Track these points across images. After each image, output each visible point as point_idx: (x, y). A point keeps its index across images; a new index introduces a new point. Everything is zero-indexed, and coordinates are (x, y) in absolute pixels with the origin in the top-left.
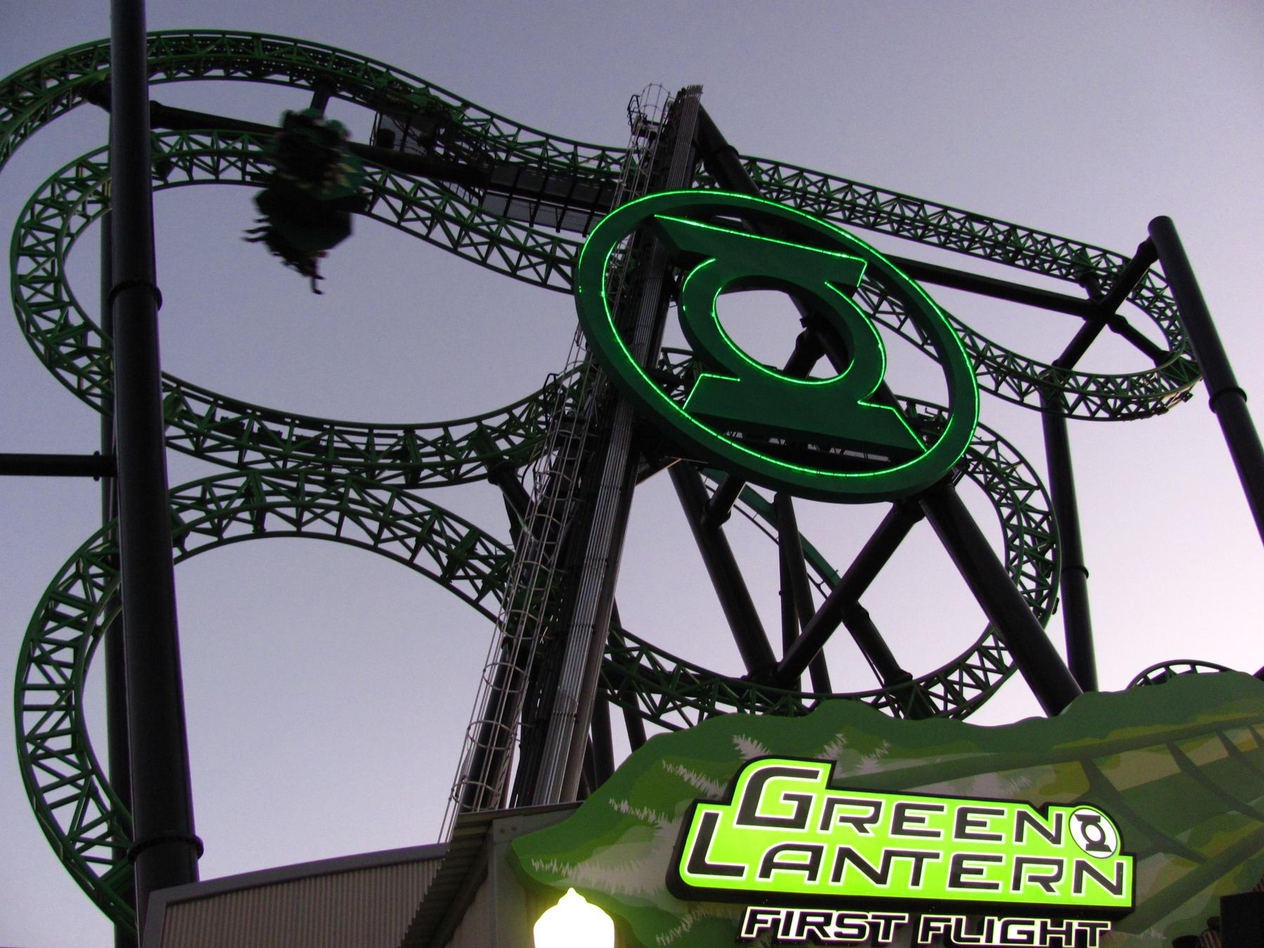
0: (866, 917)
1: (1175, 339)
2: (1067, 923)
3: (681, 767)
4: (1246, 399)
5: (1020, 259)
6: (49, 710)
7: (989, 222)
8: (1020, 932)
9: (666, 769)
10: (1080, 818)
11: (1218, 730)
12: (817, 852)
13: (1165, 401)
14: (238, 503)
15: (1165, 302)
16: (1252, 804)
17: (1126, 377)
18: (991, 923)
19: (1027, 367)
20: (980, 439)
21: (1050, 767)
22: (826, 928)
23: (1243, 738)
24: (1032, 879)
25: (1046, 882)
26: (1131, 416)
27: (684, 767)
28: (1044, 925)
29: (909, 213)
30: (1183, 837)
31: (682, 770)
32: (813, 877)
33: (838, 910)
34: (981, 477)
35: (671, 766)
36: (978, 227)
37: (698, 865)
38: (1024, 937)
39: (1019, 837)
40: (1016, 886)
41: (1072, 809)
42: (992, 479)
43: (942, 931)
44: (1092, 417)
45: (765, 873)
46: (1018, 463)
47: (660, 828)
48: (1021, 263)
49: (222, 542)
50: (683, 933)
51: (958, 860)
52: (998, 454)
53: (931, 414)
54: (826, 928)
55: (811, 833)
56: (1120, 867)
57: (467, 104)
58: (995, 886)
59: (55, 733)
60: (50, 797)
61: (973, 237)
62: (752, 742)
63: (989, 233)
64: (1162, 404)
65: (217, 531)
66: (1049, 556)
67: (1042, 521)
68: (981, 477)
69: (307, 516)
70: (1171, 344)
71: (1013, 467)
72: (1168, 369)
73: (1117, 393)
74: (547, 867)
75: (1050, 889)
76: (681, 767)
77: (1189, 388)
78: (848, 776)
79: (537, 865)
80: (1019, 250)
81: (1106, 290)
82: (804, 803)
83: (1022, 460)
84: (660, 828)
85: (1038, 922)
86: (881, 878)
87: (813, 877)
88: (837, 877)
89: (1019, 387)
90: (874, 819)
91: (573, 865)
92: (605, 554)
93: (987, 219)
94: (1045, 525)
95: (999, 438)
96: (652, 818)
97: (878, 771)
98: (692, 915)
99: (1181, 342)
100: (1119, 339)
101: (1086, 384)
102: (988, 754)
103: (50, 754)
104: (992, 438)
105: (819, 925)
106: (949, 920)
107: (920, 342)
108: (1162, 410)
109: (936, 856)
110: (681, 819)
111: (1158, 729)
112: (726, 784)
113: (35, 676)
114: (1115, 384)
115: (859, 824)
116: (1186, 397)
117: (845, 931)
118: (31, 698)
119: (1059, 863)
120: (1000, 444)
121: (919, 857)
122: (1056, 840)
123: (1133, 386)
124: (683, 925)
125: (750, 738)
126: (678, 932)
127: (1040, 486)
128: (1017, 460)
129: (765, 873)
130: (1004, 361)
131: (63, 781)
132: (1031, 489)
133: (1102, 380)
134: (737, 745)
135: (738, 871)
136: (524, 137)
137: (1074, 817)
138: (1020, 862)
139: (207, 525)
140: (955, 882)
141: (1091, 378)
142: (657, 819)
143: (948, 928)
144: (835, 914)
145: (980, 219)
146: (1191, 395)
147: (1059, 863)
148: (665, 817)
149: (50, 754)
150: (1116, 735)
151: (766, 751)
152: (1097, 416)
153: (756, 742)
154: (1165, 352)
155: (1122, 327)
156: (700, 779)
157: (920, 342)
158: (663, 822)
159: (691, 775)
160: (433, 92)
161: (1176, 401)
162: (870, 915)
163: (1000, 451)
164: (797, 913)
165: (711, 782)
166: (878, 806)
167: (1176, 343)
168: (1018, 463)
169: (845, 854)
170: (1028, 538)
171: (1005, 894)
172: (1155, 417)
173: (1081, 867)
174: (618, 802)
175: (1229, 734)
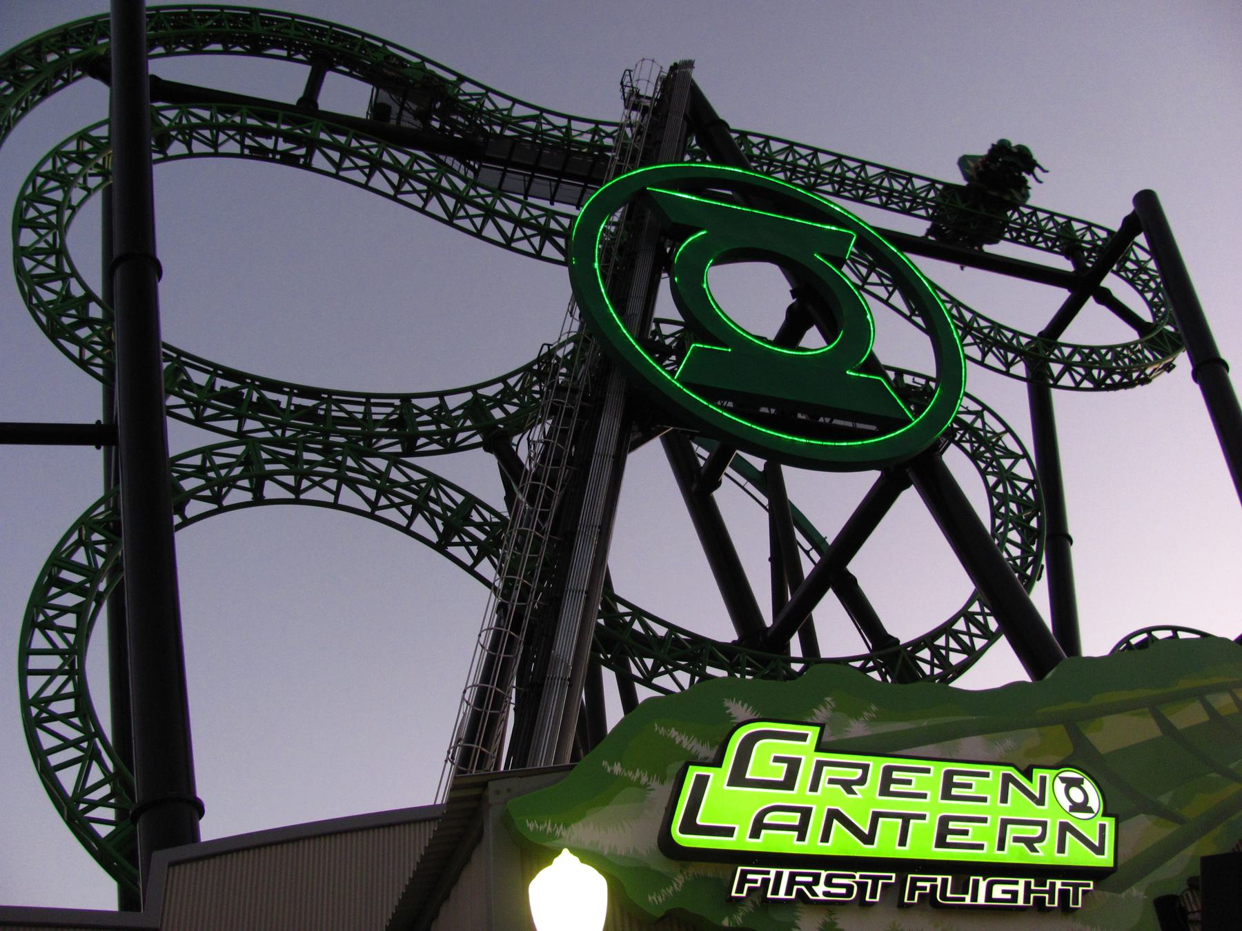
0: (854, 877)
1: (1159, 311)
2: (1050, 883)
3: (673, 729)
6: (52, 674)
8: (1004, 892)
10: (1063, 780)
12: (806, 813)
13: (1148, 371)
14: (237, 471)
17: (1110, 348)
18: (976, 883)
19: (1013, 338)
20: (967, 408)
21: (1034, 730)
24: (1016, 839)
25: (1030, 843)
26: (1115, 387)
27: (676, 730)
28: (1027, 885)
29: (897, 187)
31: (673, 733)
32: (802, 837)
33: (826, 871)
34: (967, 446)
35: (662, 728)
37: (690, 826)
38: (1009, 896)
39: (1004, 799)
40: (1001, 847)
42: (978, 448)
43: (928, 891)
44: (1077, 387)
45: (755, 834)
46: (1004, 433)
47: (652, 790)
49: (222, 509)
51: (944, 821)
52: (984, 423)
53: (919, 384)
55: (800, 795)
57: (462, 79)
59: (58, 696)
60: (54, 760)
62: (742, 705)
64: (1145, 374)
65: (217, 498)
66: (1034, 523)
67: (1027, 489)
68: (967, 446)
69: (305, 483)
70: (1154, 315)
71: (999, 436)
73: (1102, 364)
74: (541, 828)
75: (1034, 850)
76: (673, 729)
78: (836, 739)
79: (531, 826)
81: (1090, 262)
82: (794, 765)
83: (1008, 430)
84: (652, 790)
85: (1022, 881)
86: (868, 839)
87: (802, 837)
89: (1006, 357)
91: (566, 826)
92: (598, 521)
94: (1030, 493)
95: (985, 408)
96: (644, 779)
97: (868, 733)
98: (684, 876)
100: (1104, 311)
101: (1071, 355)
102: (974, 718)
103: (54, 717)
104: (979, 408)
105: (809, 886)
106: (935, 880)
108: (1146, 381)
113: (39, 641)
114: (1099, 355)
115: (847, 785)
116: (1169, 368)
118: (35, 662)
119: (1043, 824)
120: (986, 413)
121: (906, 819)
122: (1040, 801)
124: (675, 885)
125: (740, 702)
127: (1025, 455)
129: (755, 834)
130: (990, 332)
131: (67, 744)
132: (1017, 458)
133: (1086, 351)
134: (728, 708)
136: (519, 111)
138: (1005, 823)
139: (207, 493)
140: (941, 843)
141: (1076, 349)
143: (934, 888)
144: (824, 874)
146: (1174, 366)
147: (1043, 824)
148: (657, 779)
149: (54, 717)
151: (756, 715)
153: (746, 705)
154: (1149, 324)
155: (1107, 299)
156: (693, 739)
157: (908, 313)
158: (655, 784)
160: (429, 66)
161: (1159, 372)
162: (857, 875)
164: (786, 873)
166: (865, 768)
167: (1160, 315)
168: (1004, 433)
169: (833, 815)
170: (1013, 506)
171: (988, 854)
173: (1065, 828)
174: (611, 764)
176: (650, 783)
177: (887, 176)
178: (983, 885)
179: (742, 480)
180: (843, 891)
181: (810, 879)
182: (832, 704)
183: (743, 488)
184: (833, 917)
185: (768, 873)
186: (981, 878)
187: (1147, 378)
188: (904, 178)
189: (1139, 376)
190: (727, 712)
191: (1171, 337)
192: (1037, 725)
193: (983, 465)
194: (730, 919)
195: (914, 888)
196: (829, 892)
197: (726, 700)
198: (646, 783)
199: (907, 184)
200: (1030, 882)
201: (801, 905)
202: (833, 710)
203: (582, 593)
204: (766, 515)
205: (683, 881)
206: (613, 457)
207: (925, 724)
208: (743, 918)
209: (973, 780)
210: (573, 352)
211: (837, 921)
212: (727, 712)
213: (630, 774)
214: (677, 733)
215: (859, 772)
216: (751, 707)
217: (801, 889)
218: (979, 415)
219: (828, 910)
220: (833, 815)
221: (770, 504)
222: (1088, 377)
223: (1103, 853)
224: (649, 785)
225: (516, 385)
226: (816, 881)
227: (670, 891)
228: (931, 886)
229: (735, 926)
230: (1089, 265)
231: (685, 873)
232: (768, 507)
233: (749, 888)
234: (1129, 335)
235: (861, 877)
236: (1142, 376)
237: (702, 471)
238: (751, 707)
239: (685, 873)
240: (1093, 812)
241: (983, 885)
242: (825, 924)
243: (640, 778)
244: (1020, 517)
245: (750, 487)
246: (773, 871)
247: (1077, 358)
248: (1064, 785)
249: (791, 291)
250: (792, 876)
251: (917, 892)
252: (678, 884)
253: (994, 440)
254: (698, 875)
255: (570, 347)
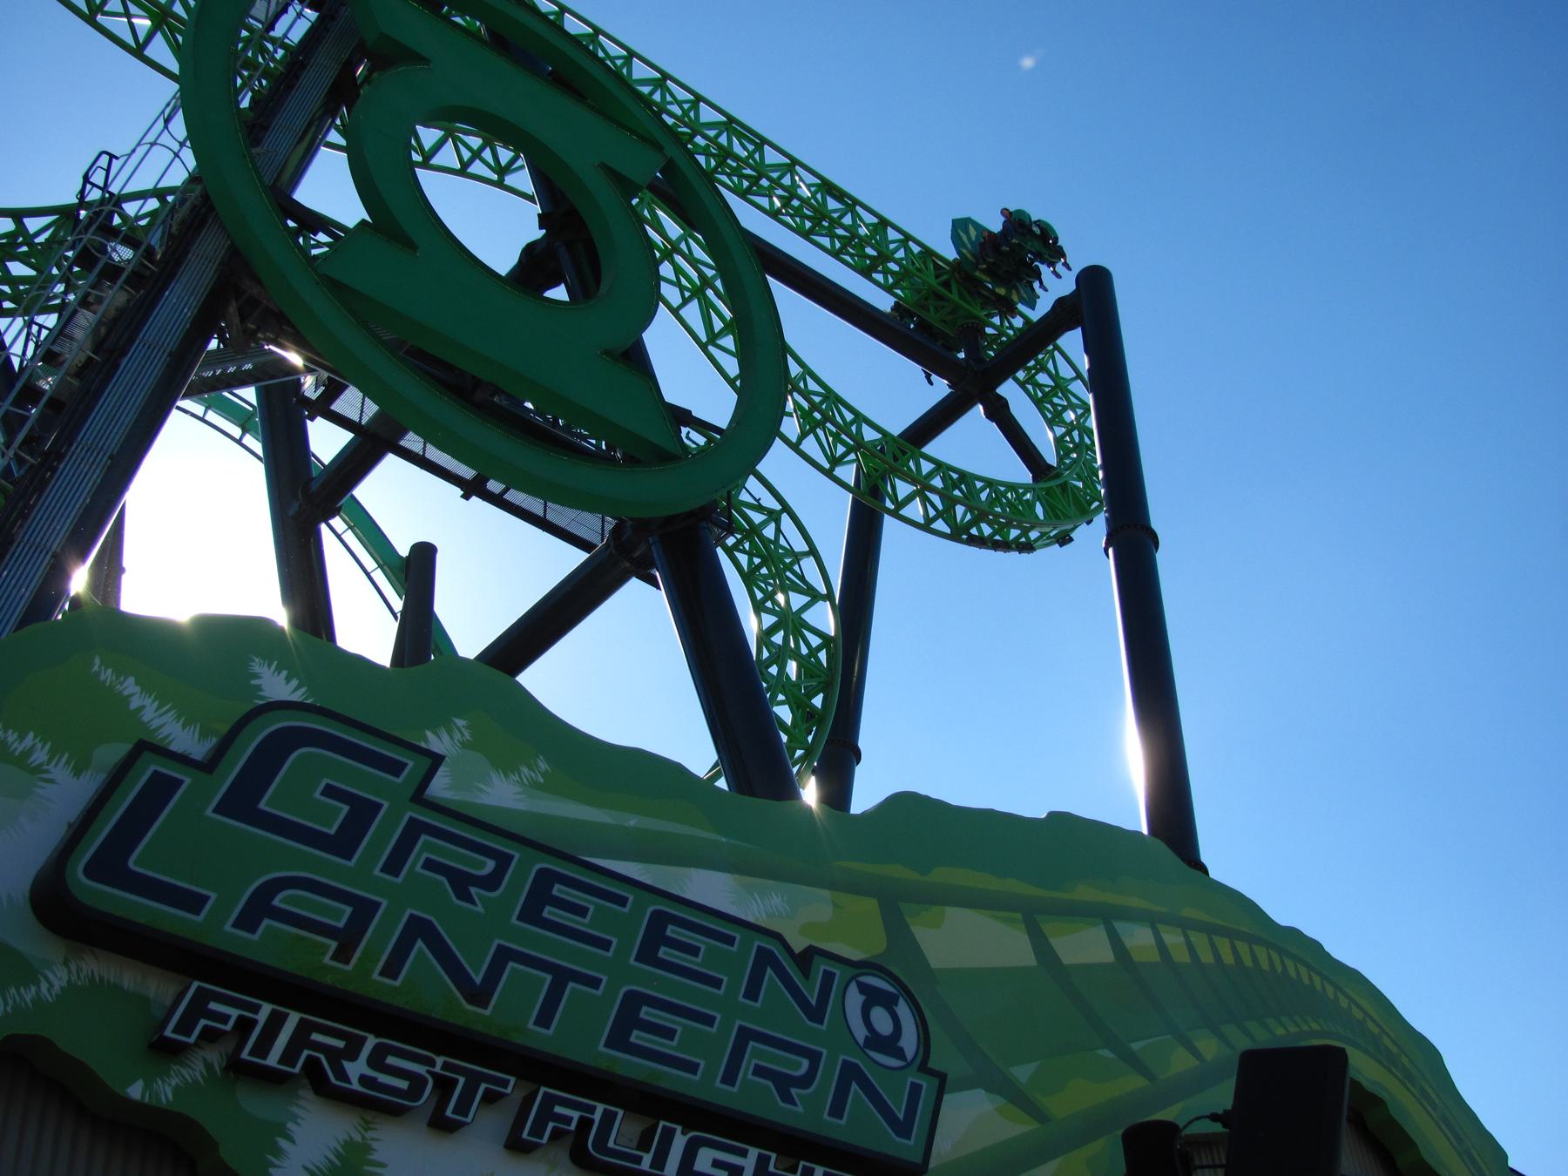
0: (432, 1063)
1: (1067, 455)
2: (805, 1168)
3: (131, 680)
4: (1157, 548)
5: (879, 272)
7: (851, 203)
9: (98, 673)
10: (863, 988)
11: (1107, 916)
12: (364, 910)
13: (1033, 535)
15: (1068, 399)
16: (1136, 1046)
17: (990, 483)
18: (668, 1136)
19: (852, 422)
20: (758, 501)
21: (826, 893)
22: (347, 1065)
23: (1139, 939)
24: (760, 1071)
25: (784, 1084)
26: (980, 542)
27: (136, 684)
28: (762, 1161)
29: (737, 148)
30: (1022, 1073)
31: (130, 686)
32: (343, 954)
33: (377, 1036)
34: (743, 559)
35: (109, 671)
36: (832, 204)
37: (109, 866)
39: (752, 993)
40: (730, 1078)
41: (855, 971)
42: (759, 567)
43: (573, 1127)
44: (926, 526)
45: (248, 920)
46: (805, 554)
47: (51, 781)
48: (879, 277)
50: (38, 1000)
51: (633, 1001)
52: (778, 531)
53: (694, 442)
54: (347, 1065)
56: (915, 1090)
58: (692, 1068)
61: (820, 215)
62: (288, 680)
63: (847, 220)
64: (1028, 538)
66: (818, 701)
67: (819, 648)
68: (743, 559)
70: (1060, 459)
71: (798, 557)
72: (1049, 491)
73: (970, 500)
75: (789, 1099)
76: (131, 680)
77: (1072, 526)
80: (884, 257)
81: (993, 350)
82: (362, 812)
83: (813, 552)
84: (51, 781)
85: (754, 1153)
87: (343, 954)
88: (391, 970)
89: (833, 448)
90: (491, 882)
93: (850, 197)
94: (823, 656)
95: (786, 508)
96: (40, 756)
97: (521, 806)
98: (70, 972)
99: (1074, 461)
101: (931, 475)
102: (724, 840)
104: (778, 507)
105: (335, 1056)
106: (592, 1110)
107: (704, 339)
108: (1028, 547)
109: (594, 983)
110: (102, 777)
111: (1014, 886)
112: (214, 740)
114: (970, 486)
115: (462, 883)
116: (1064, 539)
117: (384, 1079)
119: (814, 1057)
120: (785, 518)
121: (562, 977)
122: (816, 1014)
123: (995, 500)
124: (44, 986)
125: (285, 673)
126: (28, 998)
127: (829, 596)
128: (806, 548)
129: (248, 920)
130: (822, 403)
132: (815, 596)
133: (955, 476)
134: (256, 676)
135: (194, 902)
137: (853, 988)
138: (745, 1035)
140: (618, 1039)
141: (940, 466)
142: (48, 764)
143: (585, 1124)
144: (371, 1041)
145: (840, 195)
146: (1071, 540)
147: (814, 1057)
148: (68, 762)
150: (942, 875)
152: (934, 526)
153: (294, 682)
154: (1050, 467)
155: (1000, 414)
156: (166, 712)
157: (704, 339)
158: (60, 772)
159: (148, 701)
161: (1048, 541)
162: (440, 1060)
163: (783, 528)
164: (294, 1018)
165: (184, 726)
167: (1067, 461)
168: (805, 554)
169: (418, 928)
170: (792, 668)
171: (705, 1085)
172: (1014, 554)
173: (850, 1073)
175: (1119, 926)
176: (51, 767)
177: (727, 130)
178: (679, 1142)
179: (370, 564)
180: (403, 1084)
181: (340, 1044)
182: (466, 734)
183: (368, 575)
184: (370, 1134)
185: (256, 1009)
186: (679, 1129)
187: (1031, 545)
188: (751, 142)
189: (1019, 537)
190: (254, 682)
191: (1075, 490)
192: (833, 886)
193: (759, 595)
194: (148, 1086)
195: (546, 1114)
196: (374, 1080)
197: (257, 660)
198: (42, 764)
199: (755, 151)
200: (769, 1158)
201: (307, 1094)
202: (464, 745)
203: (47, 554)
204: (394, 626)
205: (64, 984)
206: (169, 355)
207: (632, 823)
208: (176, 1090)
209: (704, 943)
210: (153, 214)
211: (375, 1145)
212: (254, 682)
213: (12, 737)
214: (138, 689)
215: (490, 865)
216: (304, 689)
217: (318, 1060)
218: (773, 516)
219: (363, 1119)
220: (418, 928)
221: (404, 612)
222: (947, 514)
223: (908, 1136)
224: (47, 771)
225: (38, 233)
226: (352, 1053)
227: (29, 995)
228: (581, 1119)
229: (154, 1103)
230: (992, 353)
231: (73, 968)
232: (399, 615)
233: (206, 1028)
234: (1017, 472)
235: (446, 1066)
236: (1023, 540)
237: (315, 486)
238: (304, 689)
239: (73, 968)
240: (906, 1060)
241: (679, 1142)
242: (349, 1145)
243: (32, 749)
244: (796, 685)
245: (379, 576)
246: (266, 1009)
247: (937, 482)
248: (862, 998)
249: (539, 215)
250: (303, 1029)
251: (551, 1125)
252: (51, 985)
253: (788, 561)
254: (101, 979)
255: (153, 204)
